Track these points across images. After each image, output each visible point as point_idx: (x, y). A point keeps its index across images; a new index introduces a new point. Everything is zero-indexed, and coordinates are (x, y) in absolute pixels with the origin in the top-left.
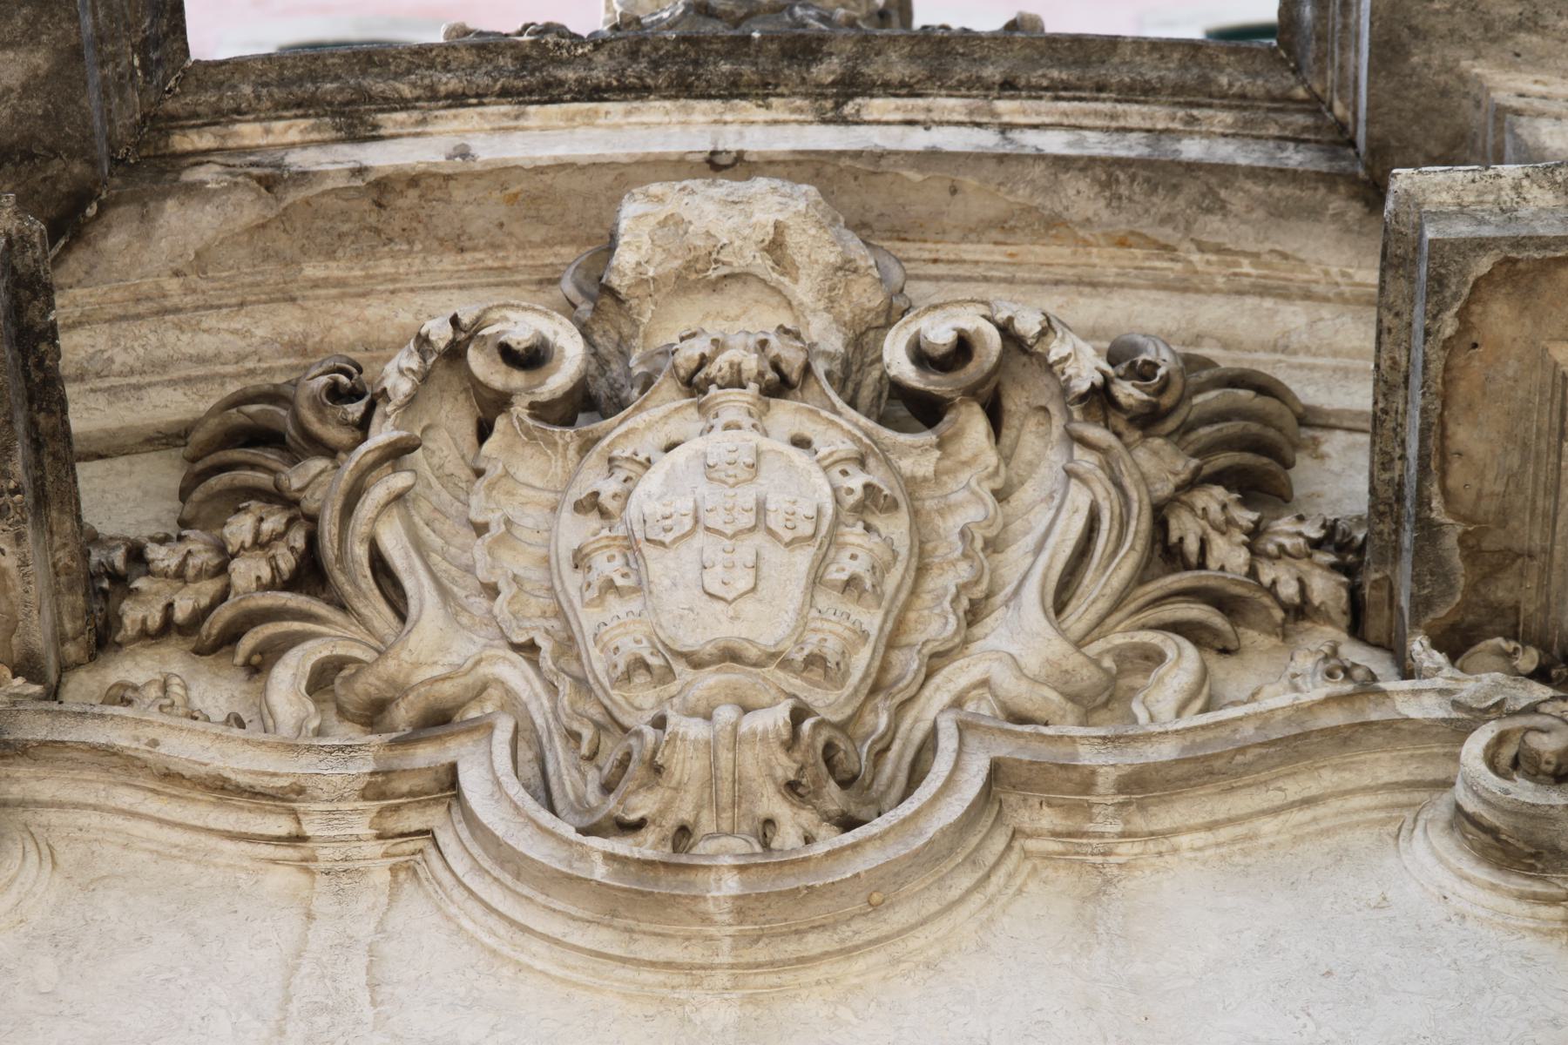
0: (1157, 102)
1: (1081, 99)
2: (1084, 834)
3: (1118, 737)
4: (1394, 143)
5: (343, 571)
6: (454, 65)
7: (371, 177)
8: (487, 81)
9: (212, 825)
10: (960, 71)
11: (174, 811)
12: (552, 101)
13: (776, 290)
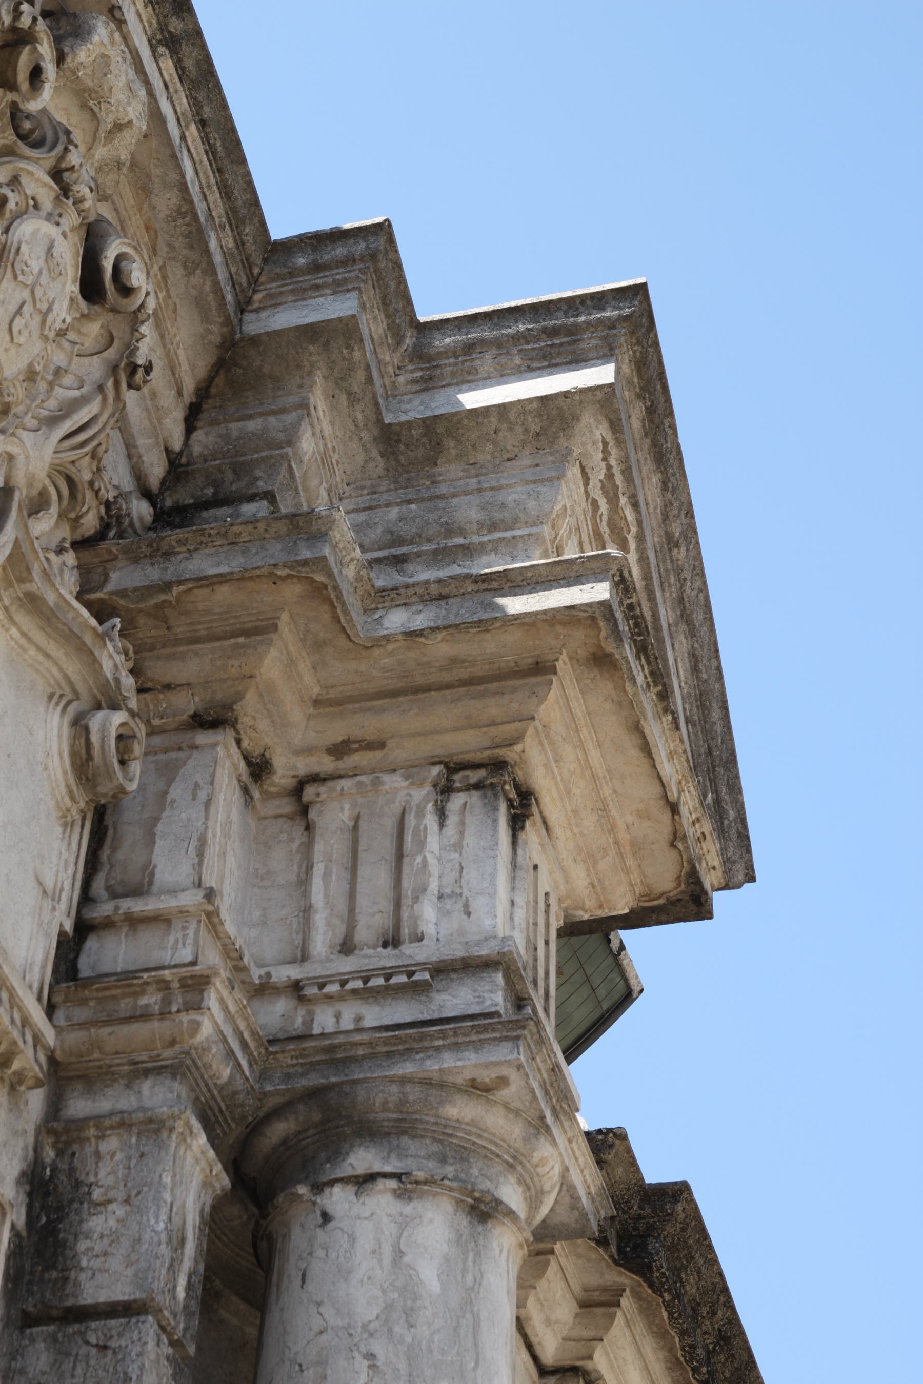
0: (224, 204)
1: (211, 165)
4: (261, 348)
10: (201, 96)
13: (94, 139)
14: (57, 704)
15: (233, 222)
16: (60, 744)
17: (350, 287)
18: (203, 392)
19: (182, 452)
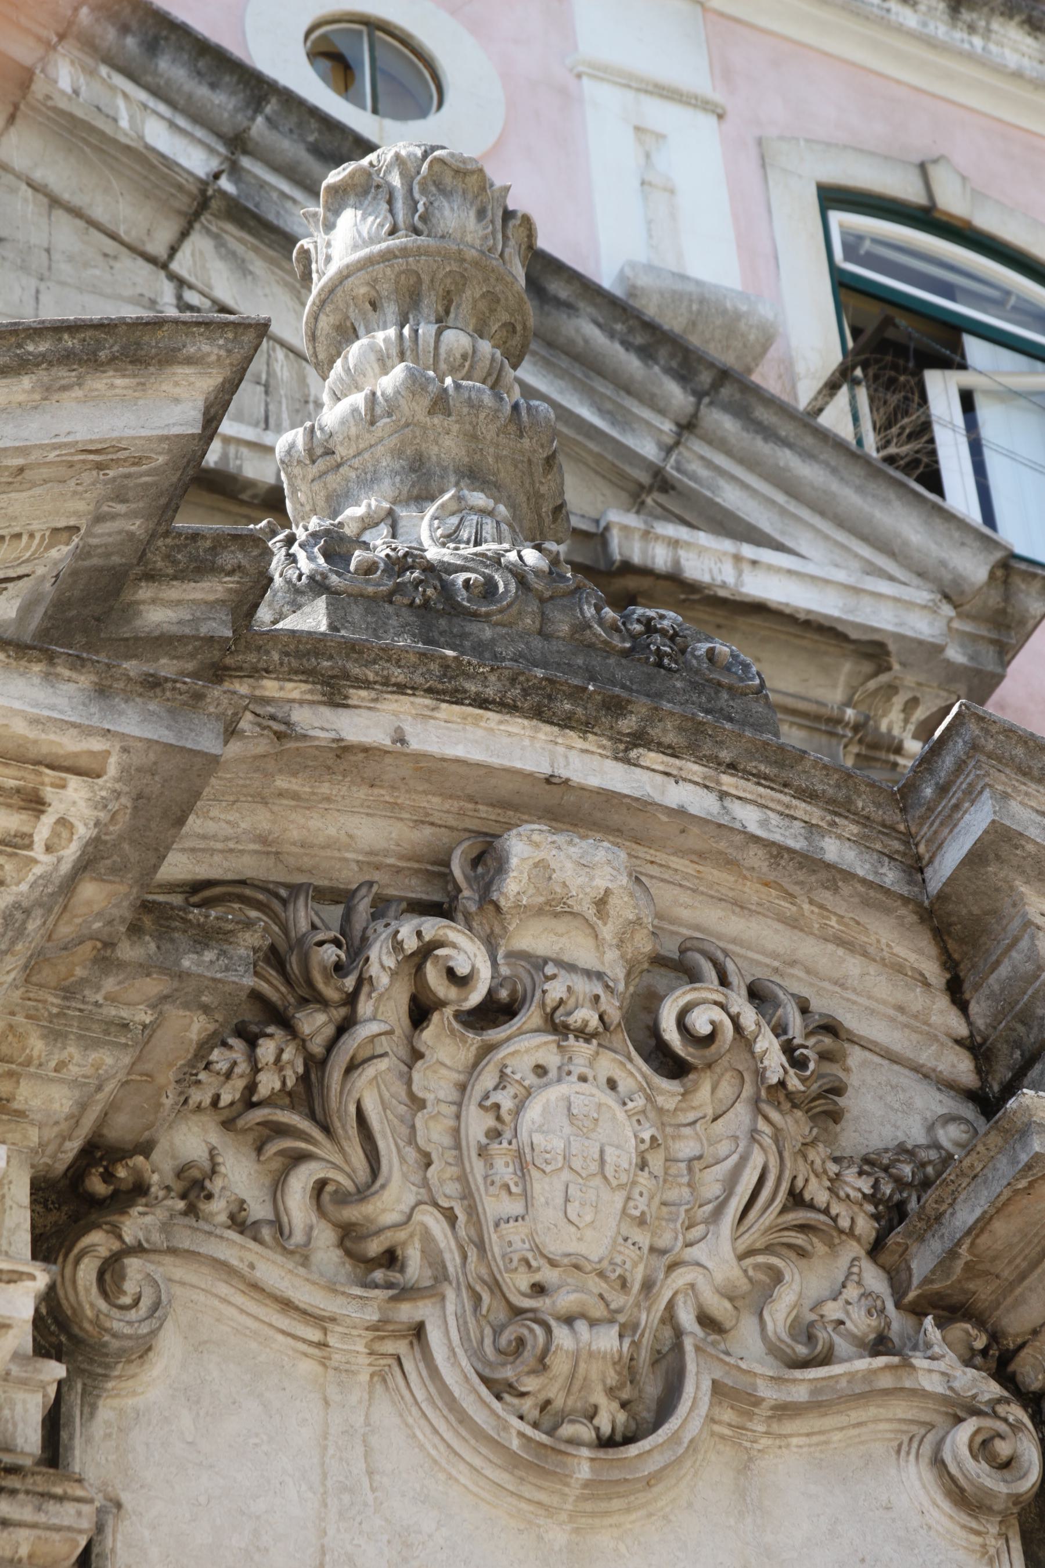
1: (772, 789)
2: (746, 1429)
3: (779, 1378)
5: (340, 1119)
6: (403, 662)
7: (343, 744)
8: (422, 680)
9: (274, 1323)
11: (252, 1307)
12: (456, 703)
14: (908, 1453)
15: (841, 811)
16: (928, 1493)
17: (979, 788)
18: (949, 963)
19: (971, 1032)
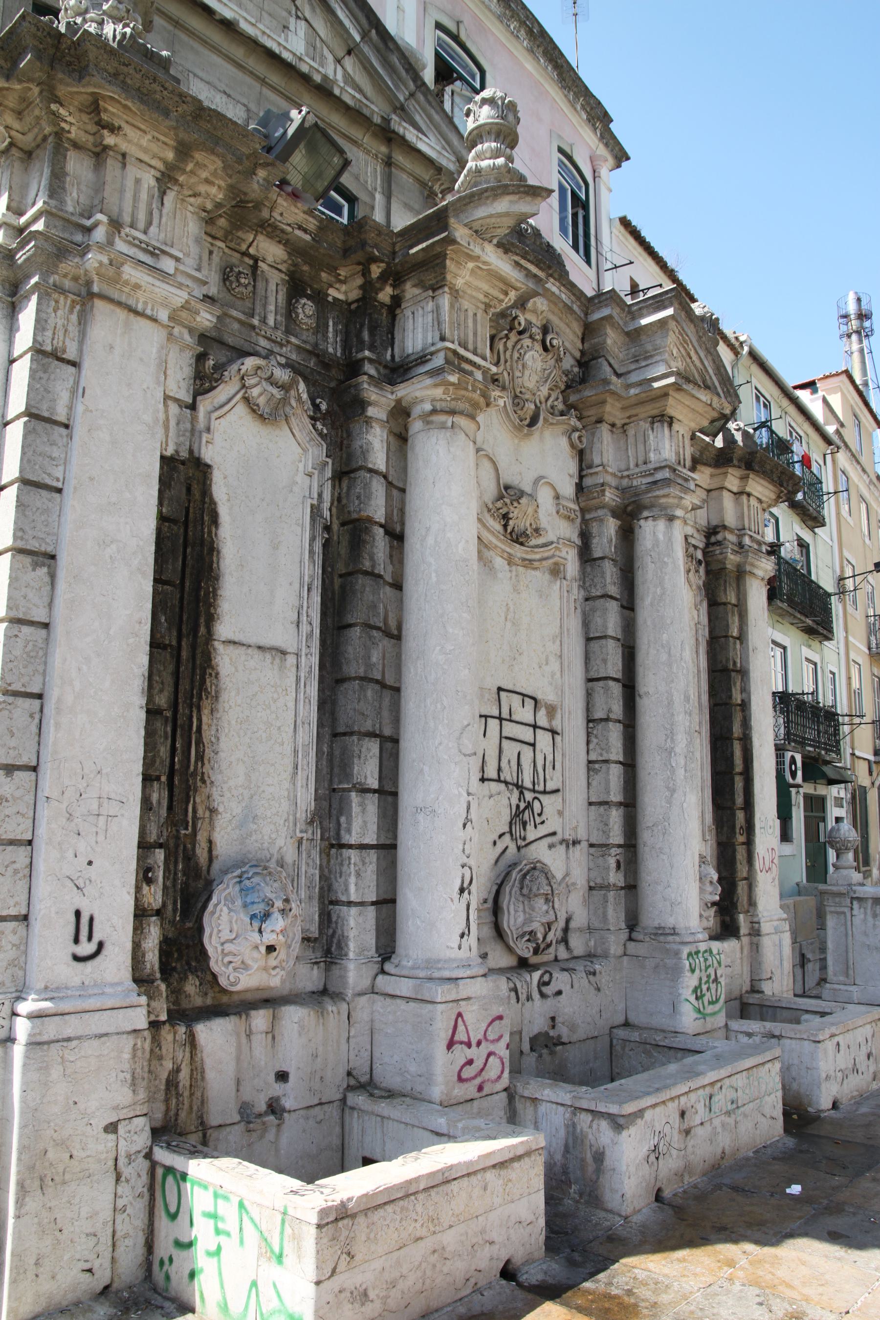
18: (584, 334)
